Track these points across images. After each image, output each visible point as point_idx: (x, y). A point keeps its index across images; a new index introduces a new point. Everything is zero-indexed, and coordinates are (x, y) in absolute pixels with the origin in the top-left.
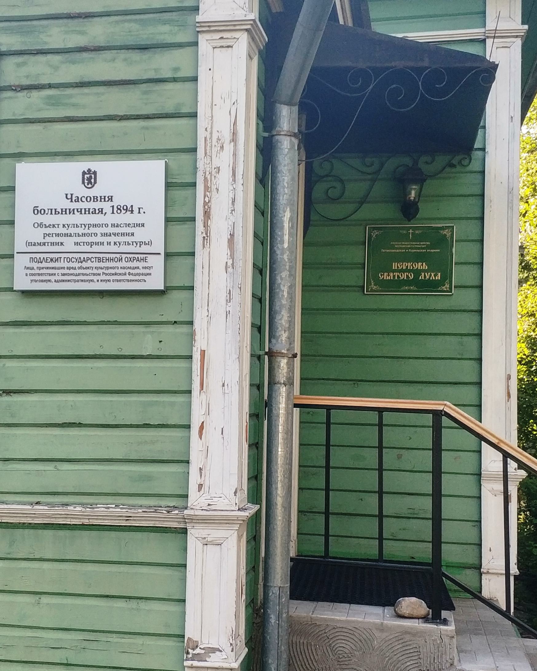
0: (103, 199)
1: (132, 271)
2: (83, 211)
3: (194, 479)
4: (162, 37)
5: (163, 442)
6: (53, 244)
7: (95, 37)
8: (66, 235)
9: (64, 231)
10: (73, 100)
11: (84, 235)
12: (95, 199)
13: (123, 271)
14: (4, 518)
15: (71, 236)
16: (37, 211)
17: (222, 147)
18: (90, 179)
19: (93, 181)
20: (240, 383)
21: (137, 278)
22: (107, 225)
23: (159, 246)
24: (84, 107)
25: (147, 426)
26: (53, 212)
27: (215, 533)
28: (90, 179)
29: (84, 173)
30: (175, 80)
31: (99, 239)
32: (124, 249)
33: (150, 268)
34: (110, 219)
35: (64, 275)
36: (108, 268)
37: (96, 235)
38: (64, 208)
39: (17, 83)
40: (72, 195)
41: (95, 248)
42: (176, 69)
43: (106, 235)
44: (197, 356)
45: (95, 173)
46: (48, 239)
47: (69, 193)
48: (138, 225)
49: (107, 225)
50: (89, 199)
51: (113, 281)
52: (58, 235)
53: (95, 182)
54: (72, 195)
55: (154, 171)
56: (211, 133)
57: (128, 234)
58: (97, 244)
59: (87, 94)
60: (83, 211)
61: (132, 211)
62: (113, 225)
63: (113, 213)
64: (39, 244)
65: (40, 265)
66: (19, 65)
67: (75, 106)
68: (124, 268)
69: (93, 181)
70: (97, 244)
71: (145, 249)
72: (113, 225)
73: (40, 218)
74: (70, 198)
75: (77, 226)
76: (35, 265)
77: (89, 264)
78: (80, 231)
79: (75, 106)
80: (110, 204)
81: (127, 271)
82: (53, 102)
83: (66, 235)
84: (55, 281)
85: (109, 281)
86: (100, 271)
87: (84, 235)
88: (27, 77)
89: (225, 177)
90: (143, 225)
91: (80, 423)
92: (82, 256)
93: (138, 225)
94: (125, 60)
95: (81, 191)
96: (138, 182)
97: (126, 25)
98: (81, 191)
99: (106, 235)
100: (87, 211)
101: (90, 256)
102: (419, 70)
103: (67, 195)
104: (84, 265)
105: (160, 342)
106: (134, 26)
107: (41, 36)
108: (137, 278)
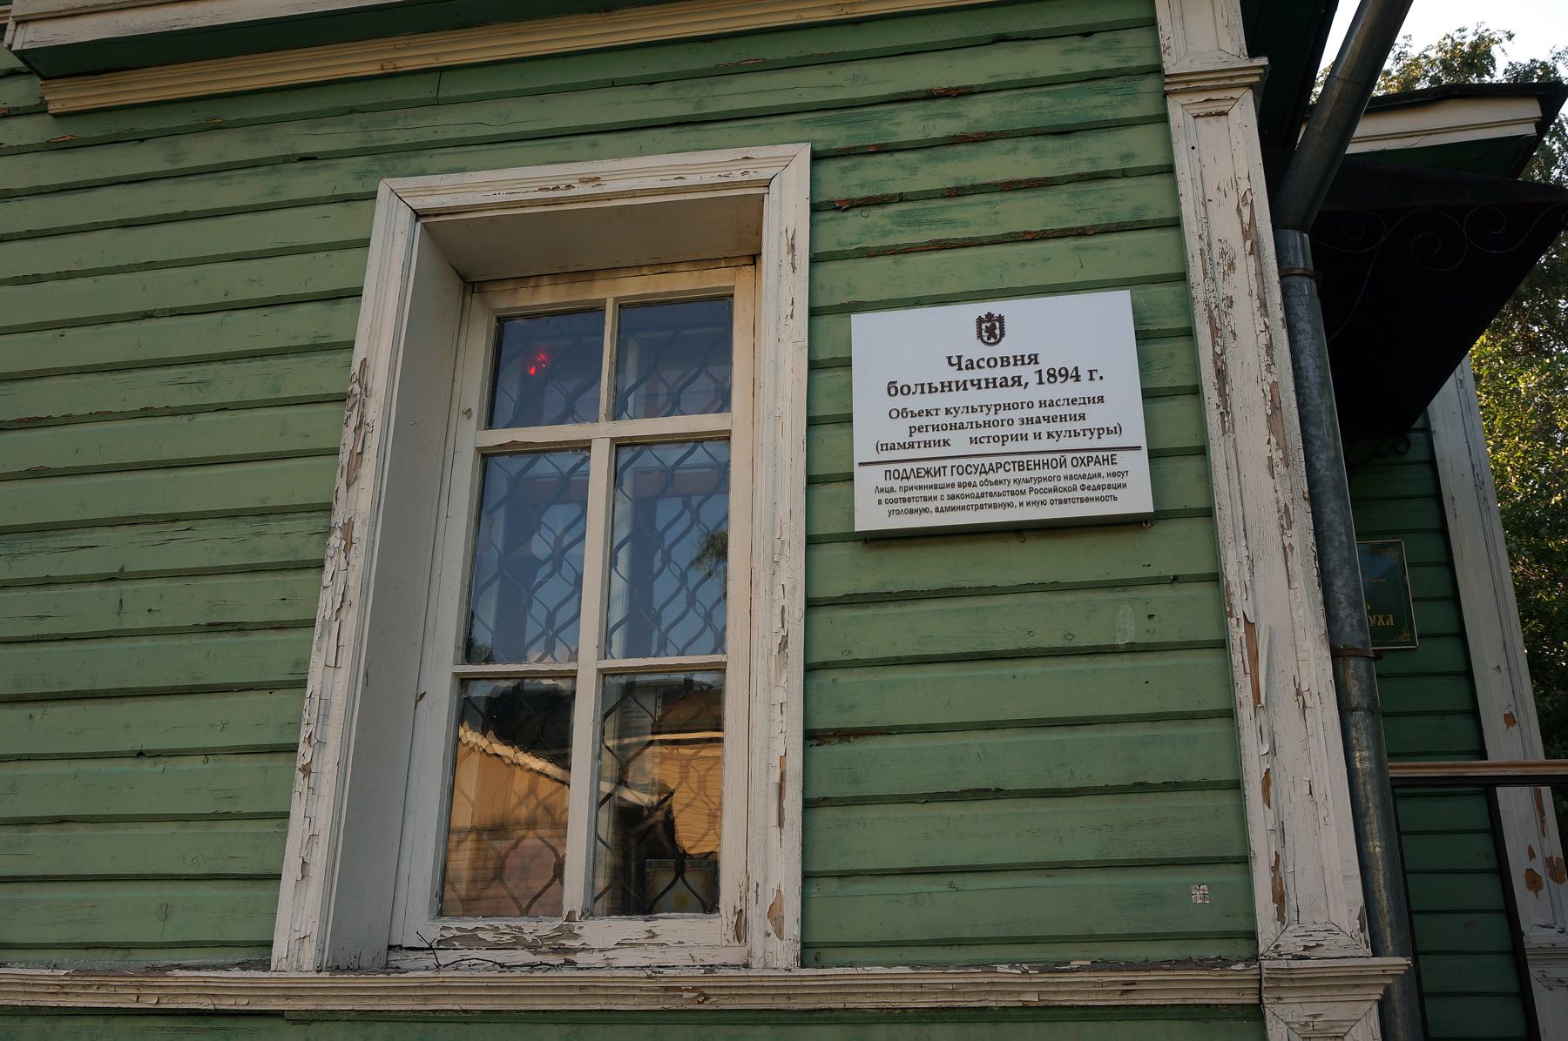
0: (1019, 360)
1: (1087, 482)
2: (983, 384)
4: (1096, 113)
5: (1185, 822)
6: (927, 444)
7: (978, 121)
8: (953, 427)
9: (949, 420)
10: (946, 216)
11: (987, 424)
12: (1005, 362)
13: (1070, 483)
14: (850, 999)
15: (962, 427)
16: (893, 389)
17: (1231, 266)
18: (991, 329)
19: (997, 332)
21: (1099, 493)
22: (1031, 405)
23: (1136, 433)
24: (966, 224)
25: (1142, 788)
26: (926, 389)
28: (991, 329)
29: (980, 321)
30: (1125, 174)
31: (1017, 429)
32: (1066, 443)
33: (1122, 474)
35: (953, 497)
36: (1039, 480)
37: (1011, 422)
38: (946, 380)
39: (844, 197)
40: (959, 358)
41: (1011, 446)
42: (1127, 157)
43: (1030, 421)
44: (1237, 633)
45: (1001, 319)
46: (917, 437)
47: (954, 354)
48: (1091, 400)
49: (1031, 405)
50: (991, 363)
51: (1052, 502)
52: (936, 428)
53: (1002, 334)
54: (959, 358)
56: (1209, 245)
57: (1073, 418)
58: (1015, 438)
59: (970, 205)
60: (983, 384)
61: (1077, 378)
62: (1042, 404)
63: (1041, 382)
64: (902, 446)
65: (905, 483)
66: (844, 170)
67: (950, 223)
68: (1071, 477)
69: (997, 332)
70: (1015, 438)
71: (1108, 441)
72: (1042, 404)
73: (900, 402)
74: (956, 362)
75: (974, 410)
76: (896, 484)
77: (1001, 475)
78: (980, 417)
79: (950, 223)
80: (1034, 367)
81: (1079, 483)
83: (953, 427)
84: (937, 510)
85: (1043, 503)
86: (1024, 487)
87: (987, 424)
88: (862, 186)
90: (1101, 399)
91: (998, 790)
92: (987, 461)
93: (1091, 400)
94: (1035, 149)
95: (977, 350)
96: (1086, 335)
97: (1033, 100)
99: (1030, 421)
100: (991, 383)
101: (1002, 460)
103: (949, 358)
104: (992, 477)
105: (1151, 616)
106: (1045, 100)
107: (885, 125)
108: (1099, 493)
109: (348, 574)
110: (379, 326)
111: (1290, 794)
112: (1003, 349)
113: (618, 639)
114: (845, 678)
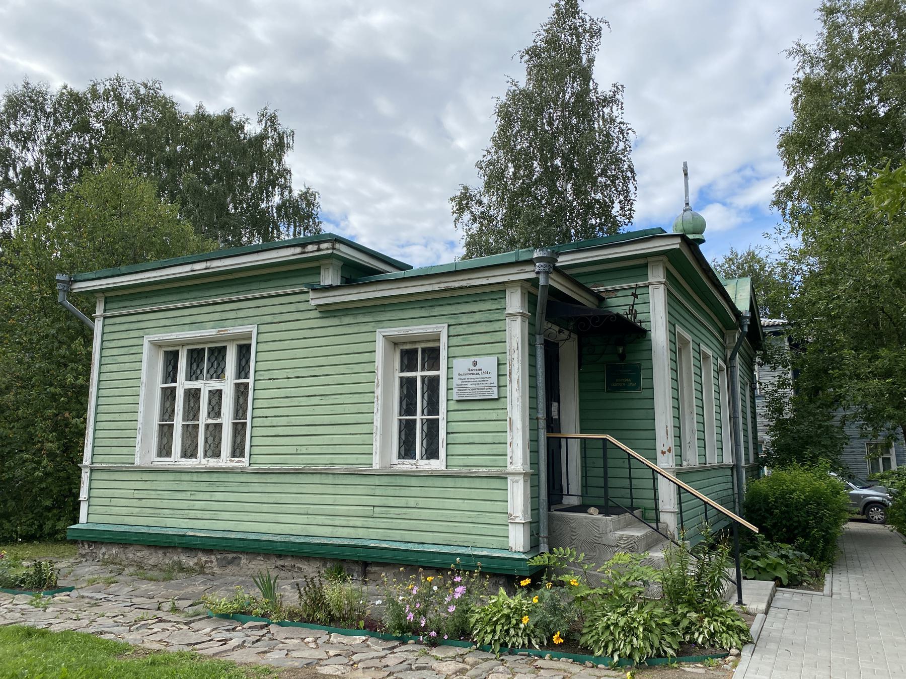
3: (509, 460)
18: (475, 363)
20: (523, 427)
27: (516, 479)
28: (475, 363)
34: (481, 376)
55: (493, 360)
74: (469, 370)
82: (464, 340)
89: (516, 360)
95: (473, 368)
96: (488, 363)
98: (473, 368)
102: (590, 317)
109: (378, 407)
110: (379, 356)
111: (514, 445)
112: (477, 368)
113: (425, 411)
114: (453, 424)
